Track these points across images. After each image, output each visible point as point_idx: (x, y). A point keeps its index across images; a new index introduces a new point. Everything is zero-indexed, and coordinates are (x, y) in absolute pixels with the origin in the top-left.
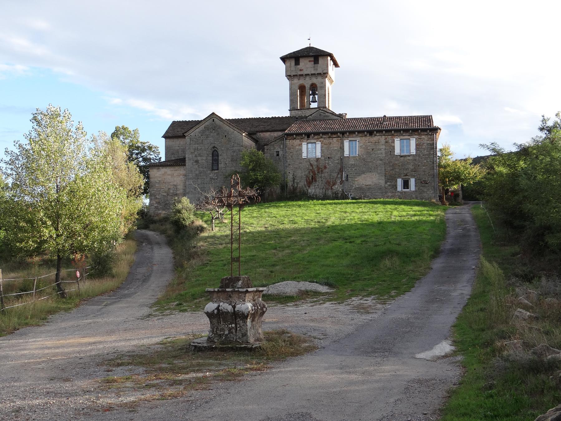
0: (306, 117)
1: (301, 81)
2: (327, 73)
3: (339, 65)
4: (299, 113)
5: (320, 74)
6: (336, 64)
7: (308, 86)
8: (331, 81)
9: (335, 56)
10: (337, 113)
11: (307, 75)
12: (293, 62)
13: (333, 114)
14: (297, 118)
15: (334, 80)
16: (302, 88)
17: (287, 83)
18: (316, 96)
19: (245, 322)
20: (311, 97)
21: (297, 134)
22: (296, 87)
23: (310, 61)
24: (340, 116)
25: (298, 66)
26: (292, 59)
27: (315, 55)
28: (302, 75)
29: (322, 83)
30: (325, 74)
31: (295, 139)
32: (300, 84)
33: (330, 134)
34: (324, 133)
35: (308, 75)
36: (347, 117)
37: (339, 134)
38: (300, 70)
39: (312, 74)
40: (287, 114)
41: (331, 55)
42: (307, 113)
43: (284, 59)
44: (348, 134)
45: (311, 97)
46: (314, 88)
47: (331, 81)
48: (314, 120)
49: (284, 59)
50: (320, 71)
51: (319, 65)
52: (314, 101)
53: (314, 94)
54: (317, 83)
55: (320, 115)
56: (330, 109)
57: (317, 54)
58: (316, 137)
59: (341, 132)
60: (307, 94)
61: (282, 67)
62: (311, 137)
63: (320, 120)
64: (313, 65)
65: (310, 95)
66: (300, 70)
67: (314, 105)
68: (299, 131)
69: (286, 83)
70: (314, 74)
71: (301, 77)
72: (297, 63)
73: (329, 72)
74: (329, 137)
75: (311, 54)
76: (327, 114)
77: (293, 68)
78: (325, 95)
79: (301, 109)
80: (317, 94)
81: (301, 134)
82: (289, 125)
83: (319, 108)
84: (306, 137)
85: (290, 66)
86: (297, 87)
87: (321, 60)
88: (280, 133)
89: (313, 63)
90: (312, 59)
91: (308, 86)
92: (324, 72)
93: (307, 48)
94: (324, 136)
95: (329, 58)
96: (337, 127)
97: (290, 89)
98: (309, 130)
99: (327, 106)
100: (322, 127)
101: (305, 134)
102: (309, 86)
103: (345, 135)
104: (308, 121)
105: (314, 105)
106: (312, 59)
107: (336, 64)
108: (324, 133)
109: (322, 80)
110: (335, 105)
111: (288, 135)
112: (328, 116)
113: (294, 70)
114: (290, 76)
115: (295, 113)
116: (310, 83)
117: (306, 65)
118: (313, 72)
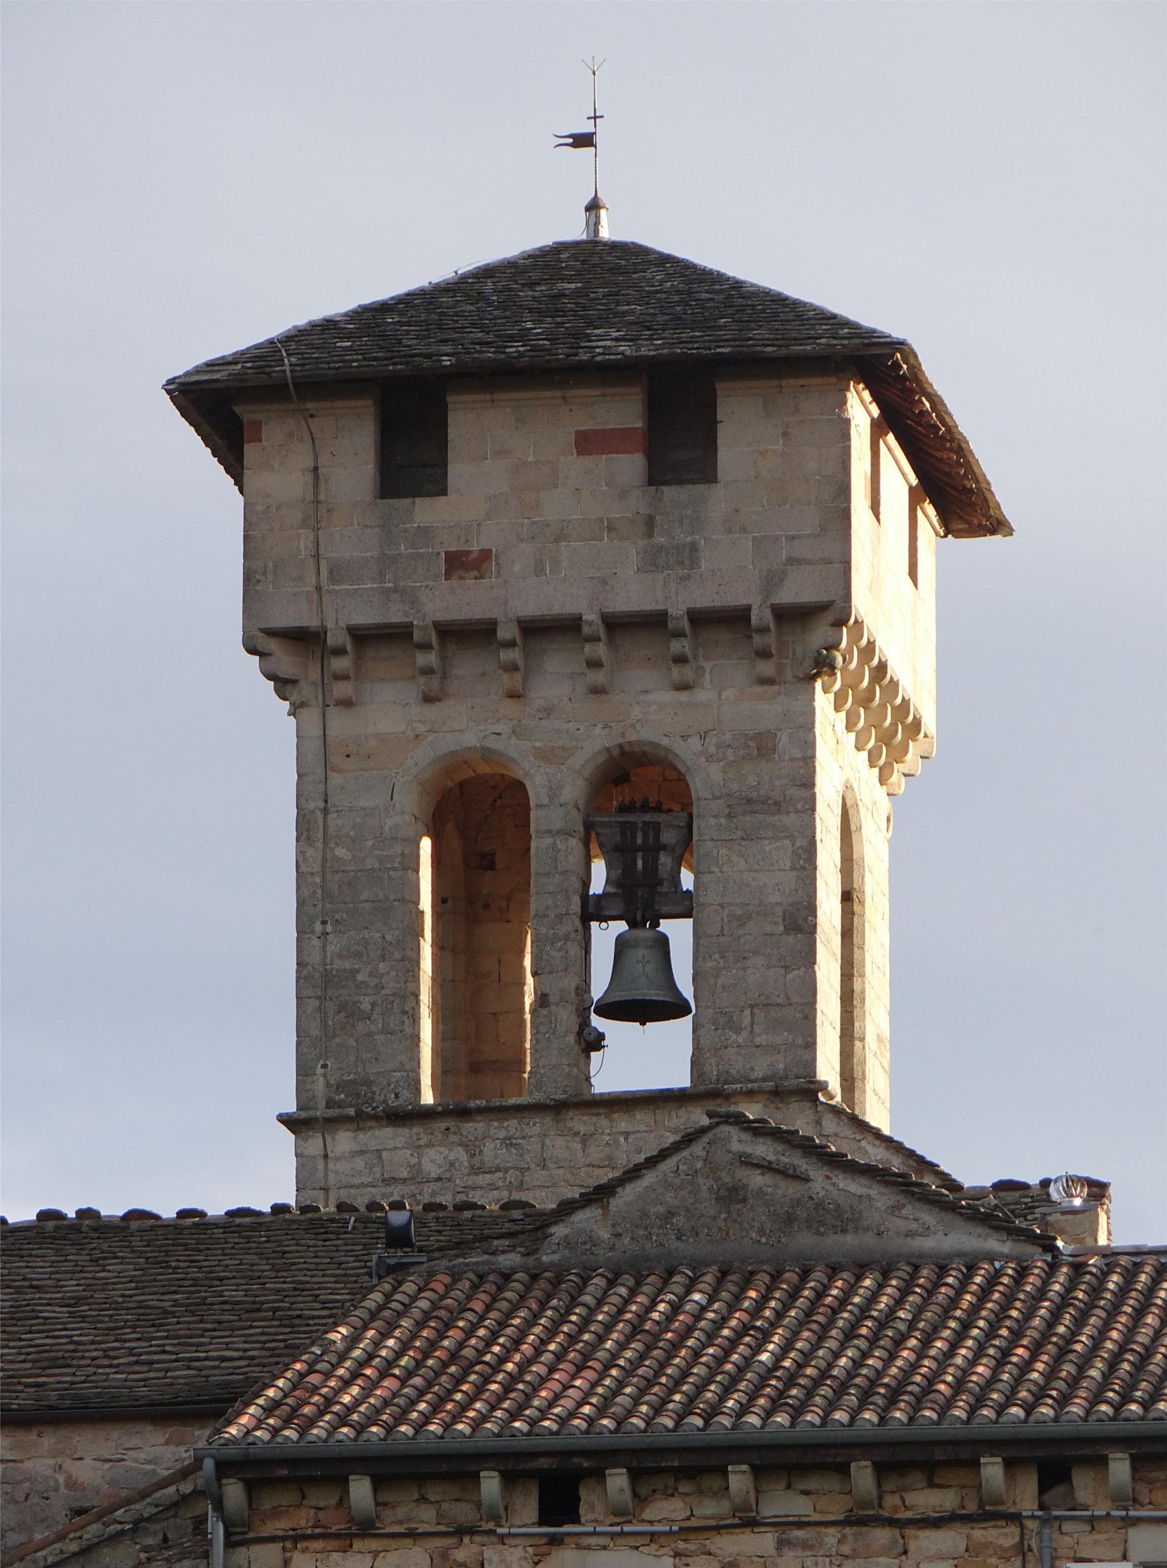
0: (531, 1226)
1: (474, 722)
2: (833, 610)
3: (825, 599)
4: (433, 1168)
5: (735, 619)
6: (955, 494)
7: (555, 792)
8: (889, 728)
9: (947, 375)
10: (974, 1171)
11: (542, 631)
12: (351, 449)
13: (914, 1180)
14: (398, 1238)
15: (926, 707)
16: (478, 817)
17: (258, 736)
18: (679, 933)
19: (373, 580)
20: (605, 936)
21: (398, 1470)
22: (394, 798)
23: (587, 443)
24: (1017, 1211)
25: (428, 511)
26: (350, 409)
27: (654, 384)
28: (474, 635)
29: (762, 746)
30: (803, 629)
31: (365, 1528)
32: (452, 764)
33: (863, 1475)
34: (781, 1461)
35: (565, 628)
36: (1113, 1230)
37: (992, 1470)
38: (459, 563)
39: (618, 625)
40: (258, 1174)
41: (883, 367)
42: (549, 1165)
43: (224, 405)
44: (1120, 1468)
45: (605, 936)
46: (644, 817)
47: (889, 728)
48: (633, 1270)
49: (224, 405)
50: (727, 575)
51: (717, 501)
52: (647, 1006)
53: (642, 899)
54: (687, 752)
55: (733, 1195)
56: (877, 1114)
57: (694, 343)
58: (667, 1510)
59: (1018, 1451)
60: (546, 894)
61: (199, 502)
62: (593, 1507)
63: (732, 1275)
64: (638, 503)
65: (594, 911)
66: (459, 563)
67: (644, 1058)
68: (432, 1428)
69: (248, 746)
70: (653, 623)
71: (468, 666)
72: (411, 462)
73: (862, 602)
74: (857, 1520)
75: (609, 343)
76: (822, 1183)
77: (353, 534)
78: (802, 921)
79: (453, 1111)
80: (685, 906)
81: (454, 1468)
82: (291, 1332)
83: (706, 1091)
84: (527, 1509)
85: (316, 513)
86: (409, 803)
87: (746, 432)
88: (154, 1452)
89: (630, 466)
90: (625, 411)
91: (555, 792)
92: (792, 593)
93: (548, 262)
94: (784, 1503)
95: (860, 408)
96: (961, 1375)
97: (246, 538)
98: (568, 1405)
99: (828, 1068)
100: (755, 1367)
101: (515, 1465)
102: (574, 790)
103: (1084, 1485)
104: (557, 1284)
105: (644, 1058)
106: (625, 411)
107: (955, 494)
108: (781, 1461)
109: (765, 710)
110: (924, 1056)
111: (259, 1471)
112: (844, 1219)
113: (368, 569)
114: (304, 639)
115: (372, 1165)
116: (594, 742)
117: (535, 498)
118: (634, 594)
